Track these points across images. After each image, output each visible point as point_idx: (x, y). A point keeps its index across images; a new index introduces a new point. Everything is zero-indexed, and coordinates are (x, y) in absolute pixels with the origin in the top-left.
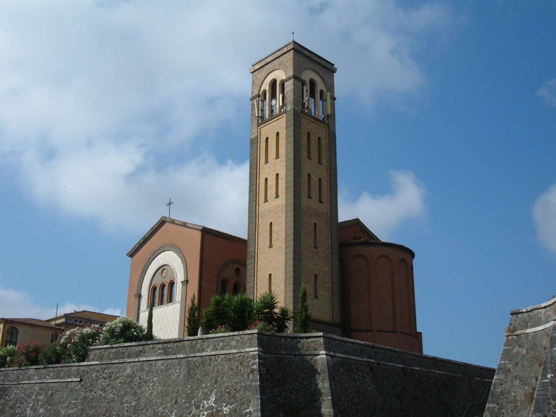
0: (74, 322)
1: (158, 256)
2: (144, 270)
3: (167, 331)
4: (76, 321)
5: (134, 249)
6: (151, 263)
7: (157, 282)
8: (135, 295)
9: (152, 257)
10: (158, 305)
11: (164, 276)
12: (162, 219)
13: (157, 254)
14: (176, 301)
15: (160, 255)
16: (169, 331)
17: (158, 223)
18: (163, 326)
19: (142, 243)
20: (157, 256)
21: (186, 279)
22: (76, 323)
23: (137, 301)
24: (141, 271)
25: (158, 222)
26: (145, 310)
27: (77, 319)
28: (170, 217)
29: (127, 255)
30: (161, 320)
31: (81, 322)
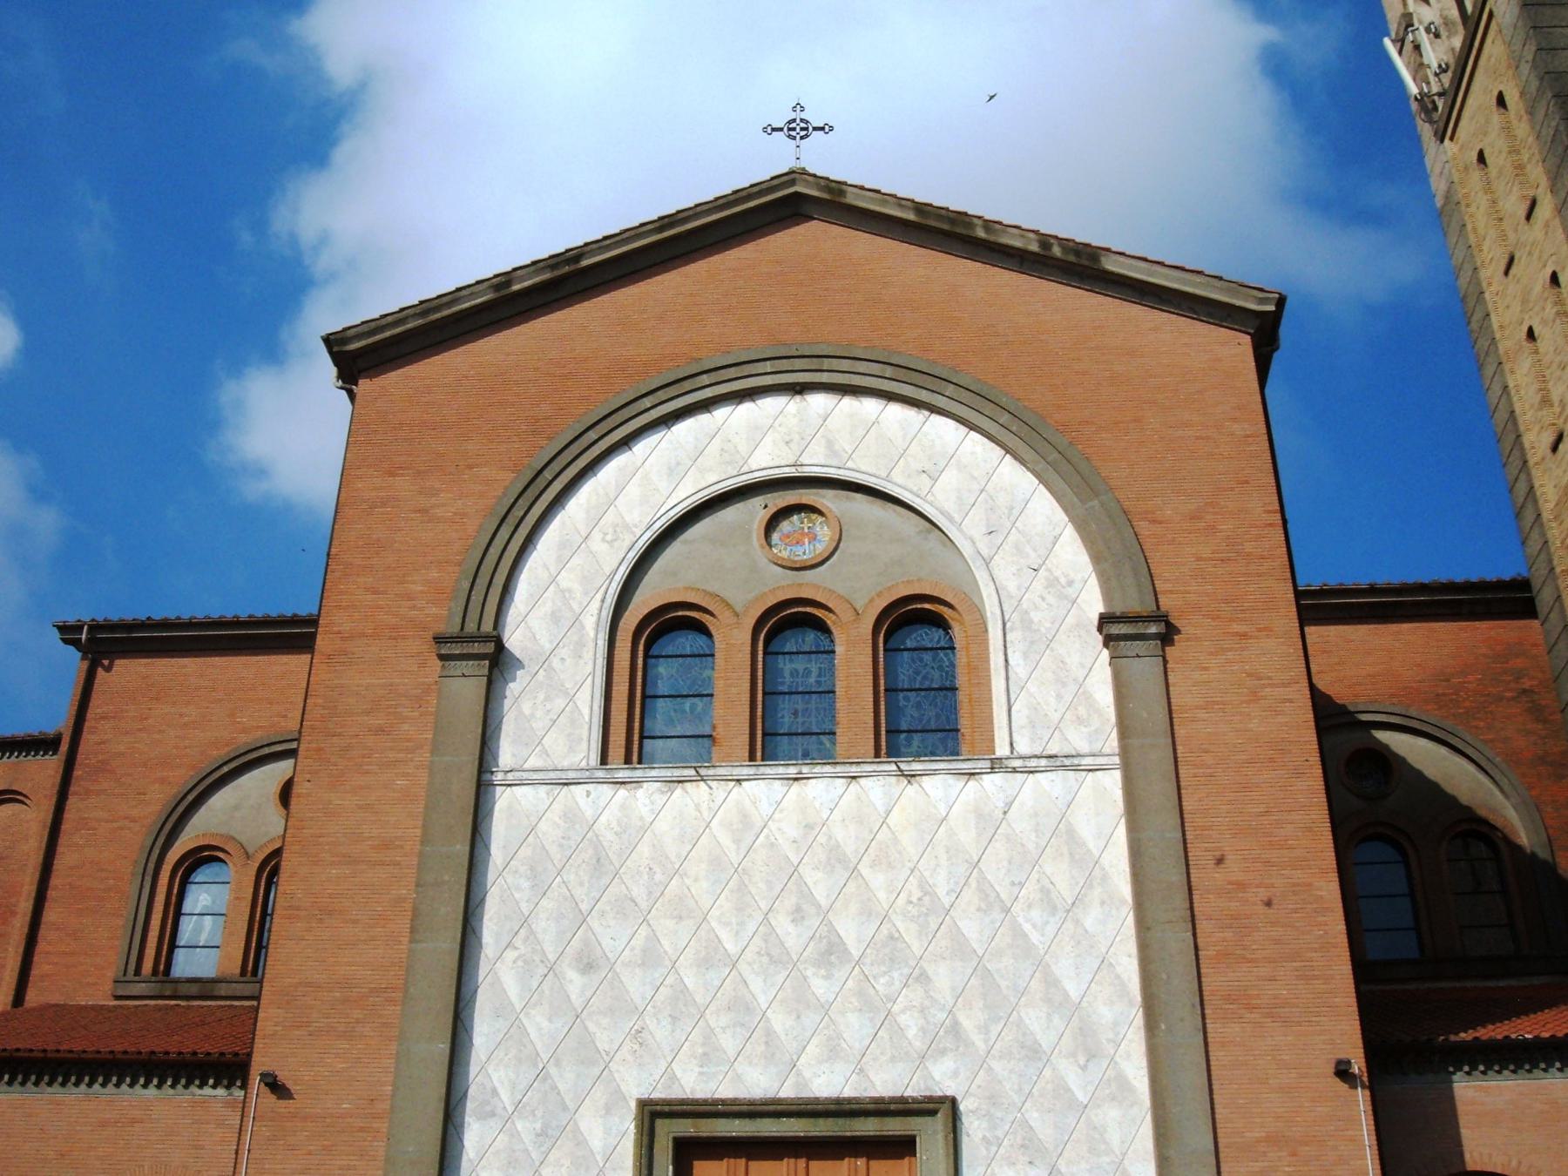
2: (548, 475)
6: (626, 443)
12: (793, 182)
16: (944, 977)
18: (851, 931)
26: (571, 775)
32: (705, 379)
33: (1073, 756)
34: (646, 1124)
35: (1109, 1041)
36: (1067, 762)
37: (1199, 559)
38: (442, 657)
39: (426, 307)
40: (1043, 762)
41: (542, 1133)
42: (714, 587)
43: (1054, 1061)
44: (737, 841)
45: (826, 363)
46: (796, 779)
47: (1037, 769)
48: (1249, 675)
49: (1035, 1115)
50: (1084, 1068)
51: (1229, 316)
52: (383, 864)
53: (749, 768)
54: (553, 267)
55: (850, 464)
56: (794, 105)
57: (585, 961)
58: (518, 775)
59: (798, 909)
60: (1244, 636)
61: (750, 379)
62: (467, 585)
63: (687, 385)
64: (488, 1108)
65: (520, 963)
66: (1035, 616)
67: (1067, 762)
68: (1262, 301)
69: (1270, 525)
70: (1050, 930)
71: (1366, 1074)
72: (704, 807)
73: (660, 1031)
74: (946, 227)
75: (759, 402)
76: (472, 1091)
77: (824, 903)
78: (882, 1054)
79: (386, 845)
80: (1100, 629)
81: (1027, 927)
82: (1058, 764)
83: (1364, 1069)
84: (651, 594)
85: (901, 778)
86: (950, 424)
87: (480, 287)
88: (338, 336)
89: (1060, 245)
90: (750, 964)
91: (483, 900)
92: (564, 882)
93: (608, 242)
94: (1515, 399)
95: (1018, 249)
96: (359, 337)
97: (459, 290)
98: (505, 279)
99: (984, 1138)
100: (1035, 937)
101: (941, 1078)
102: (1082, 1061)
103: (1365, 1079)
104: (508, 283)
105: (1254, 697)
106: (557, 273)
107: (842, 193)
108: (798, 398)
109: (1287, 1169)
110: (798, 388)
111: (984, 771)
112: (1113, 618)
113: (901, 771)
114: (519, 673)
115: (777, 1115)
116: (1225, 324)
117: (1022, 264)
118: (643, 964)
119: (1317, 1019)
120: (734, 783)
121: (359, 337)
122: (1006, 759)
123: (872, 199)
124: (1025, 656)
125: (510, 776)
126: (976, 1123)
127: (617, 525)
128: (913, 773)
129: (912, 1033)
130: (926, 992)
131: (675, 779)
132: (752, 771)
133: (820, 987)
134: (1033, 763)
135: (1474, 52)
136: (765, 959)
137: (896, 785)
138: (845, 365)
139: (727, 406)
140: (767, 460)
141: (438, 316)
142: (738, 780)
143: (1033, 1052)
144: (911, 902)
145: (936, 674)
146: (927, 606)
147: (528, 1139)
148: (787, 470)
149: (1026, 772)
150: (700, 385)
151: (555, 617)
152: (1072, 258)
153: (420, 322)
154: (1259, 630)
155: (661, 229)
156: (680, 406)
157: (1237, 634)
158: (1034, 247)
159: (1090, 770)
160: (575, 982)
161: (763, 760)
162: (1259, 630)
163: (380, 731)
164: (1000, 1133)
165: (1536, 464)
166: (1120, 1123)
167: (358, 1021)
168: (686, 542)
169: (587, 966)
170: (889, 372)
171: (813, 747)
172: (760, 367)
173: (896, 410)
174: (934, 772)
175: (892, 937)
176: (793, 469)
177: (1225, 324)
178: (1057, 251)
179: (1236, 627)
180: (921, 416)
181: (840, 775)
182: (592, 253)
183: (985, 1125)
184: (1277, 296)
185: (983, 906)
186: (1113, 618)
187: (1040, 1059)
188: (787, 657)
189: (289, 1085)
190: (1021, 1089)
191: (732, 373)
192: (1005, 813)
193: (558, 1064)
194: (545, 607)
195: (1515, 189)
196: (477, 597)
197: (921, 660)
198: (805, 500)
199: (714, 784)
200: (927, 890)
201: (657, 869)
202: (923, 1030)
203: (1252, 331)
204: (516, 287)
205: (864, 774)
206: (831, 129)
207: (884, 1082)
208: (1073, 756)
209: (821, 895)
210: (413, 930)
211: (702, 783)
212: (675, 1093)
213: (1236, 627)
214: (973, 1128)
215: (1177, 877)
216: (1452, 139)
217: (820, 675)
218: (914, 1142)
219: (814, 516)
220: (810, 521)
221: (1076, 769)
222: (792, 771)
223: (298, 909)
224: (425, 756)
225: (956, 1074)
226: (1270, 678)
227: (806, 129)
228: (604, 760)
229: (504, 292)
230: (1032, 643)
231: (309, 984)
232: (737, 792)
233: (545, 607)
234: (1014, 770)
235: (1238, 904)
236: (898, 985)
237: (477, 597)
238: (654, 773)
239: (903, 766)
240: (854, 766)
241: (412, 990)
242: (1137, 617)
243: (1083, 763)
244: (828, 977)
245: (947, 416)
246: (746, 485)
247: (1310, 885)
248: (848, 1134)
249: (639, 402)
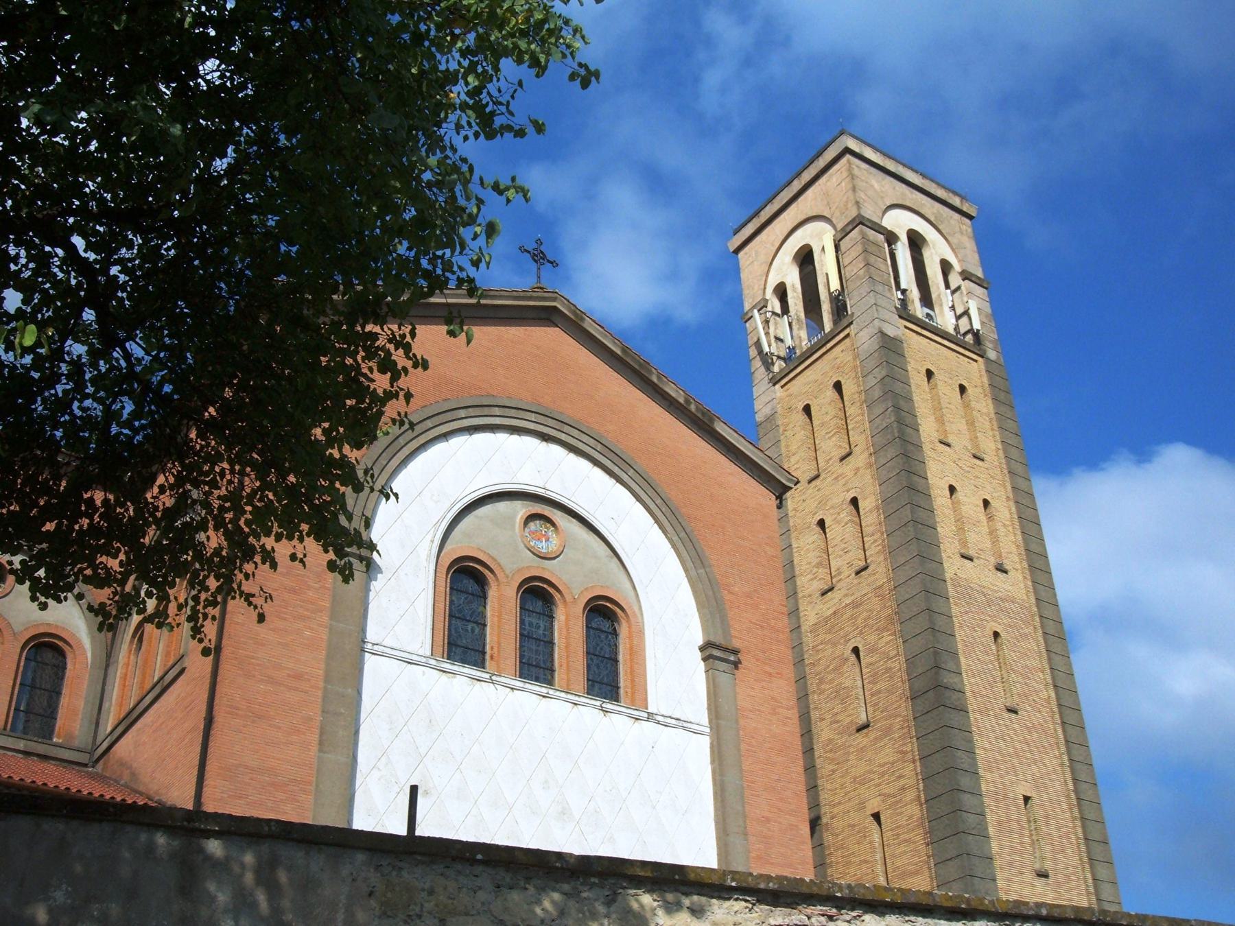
9: (462, 413)
26: (414, 657)
32: (497, 411)
36: (685, 725)
37: (751, 622)
40: (673, 721)
42: (494, 553)
45: (566, 429)
46: (544, 697)
51: (769, 481)
52: (296, 689)
58: (381, 649)
59: (546, 782)
60: (770, 674)
63: (486, 411)
67: (685, 725)
69: (783, 613)
75: (523, 437)
79: (298, 677)
80: (702, 649)
84: (459, 546)
89: (695, 405)
92: (409, 731)
94: (795, 555)
105: (774, 713)
107: (582, 319)
110: (546, 438)
114: (379, 576)
117: (669, 406)
123: (602, 333)
125: (376, 647)
132: (521, 684)
134: (668, 720)
135: (824, 350)
138: (575, 433)
142: (512, 689)
144: (606, 791)
145: (607, 649)
146: (608, 605)
152: (699, 415)
154: (778, 673)
157: (766, 672)
158: (681, 400)
161: (520, 677)
162: (778, 673)
163: (292, 591)
165: (804, 597)
167: (282, 801)
168: (476, 516)
170: (599, 447)
171: (542, 676)
174: (619, 713)
176: (543, 491)
178: (693, 408)
179: (767, 668)
188: (527, 612)
191: (512, 413)
195: (834, 439)
197: (599, 637)
198: (546, 513)
210: (321, 743)
213: (767, 668)
216: (782, 387)
217: (545, 630)
219: (548, 525)
220: (546, 528)
222: (544, 690)
223: (237, 708)
224: (325, 619)
226: (781, 703)
227: (543, 259)
231: (247, 767)
234: (658, 723)
241: (321, 786)
247: (796, 826)
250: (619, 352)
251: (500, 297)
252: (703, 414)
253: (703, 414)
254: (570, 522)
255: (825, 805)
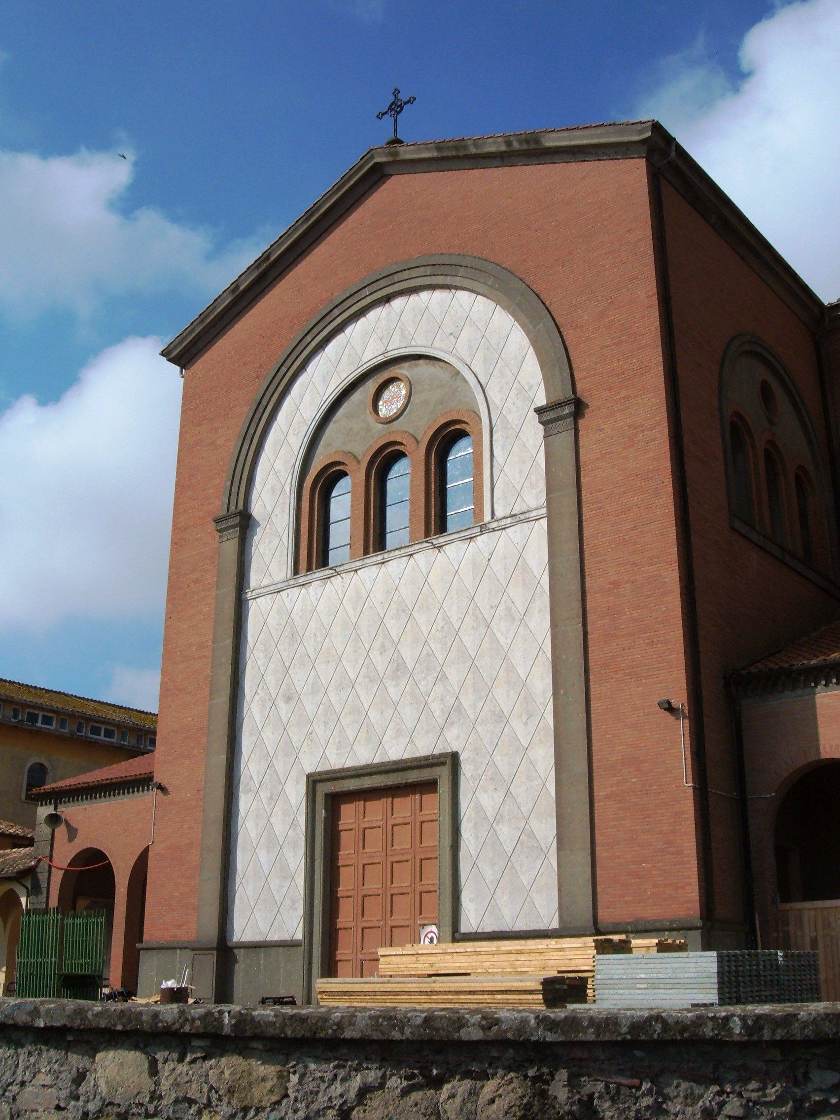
0: (91, 734)
1: (349, 330)
2: (264, 402)
3: (442, 677)
4: (96, 731)
5: (202, 321)
6: (303, 367)
7: (348, 448)
8: (217, 521)
9: (309, 338)
10: (366, 552)
11: (386, 409)
12: (372, 157)
13: (339, 320)
14: (499, 514)
15: (362, 321)
16: (454, 675)
17: (344, 184)
18: (408, 654)
19: (245, 291)
20: (340, 328)
21: (563, 392)
22: (98, 737)
23: (231, 546)
24: (246, 411)
25: (345, 179)
26: (280, 586)
27: (98, 725)
28: (348, 545)
29: (162, 354)
30: (393, 626)
31: (109, 734)
33: (525, 513)
34: (311, 787)
35: (541, 704)
36: (522, 517)
38: (219, 531)
39: (203, 316)
40: (509, 520)
41: (270, 799)
43: (510, 722)
44: (354, 609)
46: (383, 563)
47: (506, 526)
48: (629, 427)
49: (499, 758)
50: (526, 724)
53: (358, 562)
54: (258, 267)
55: (413, 343)
56: (393, 91)
57: (287, 696)
59: (383, 646)
61: (359, 303)
62: (229, 483)
63: (328, 319)
64: (248, 787)
65: (260, 702)
66: (510, 418)
67: (522, 517)
68: (641, 131)
70: (511, 635)
71: (687, 708)
72: (339, 592)
73: (320, 731)
74: (454, 153)
76: (242, 779)
77: (396, 639)
78: (422, 730)
81: (498, 635)
82: (517, 520)
83: (686, 704)
85: (435, 549)
86: (466, 293)
87: (225, 294)
88: (166, 351)
90: (360, 684)
91: (245, 669)
93: (282, 239)
95: (495, 153)
96: (176, 347)
97: (215, 300)
98: (235, 285)
99: (472, 775)
100: (502, 641)
101: (452, 741)
102: (524, 719)
103: (686, 711)
104: (237, 287)
106: (261, 270)
108: (387, 305)
109: (633, 780)
111: (477, 534)
112: (543, 409)
113: (435, 545)
115: (370, 774)
116: (627, 156)
118: (312, 693)
119: (658, 672)
120: (353, 572)
121: (176, 347)
122: (489, 523)
124: (503, 447)
126: (468, 767)
127: (300, 423)
128: (440, 545)
129: (437, 713)
130: (445, 686)
131: (325, 577)
133: (394, 692)
136: (367, 680)
137: (432, 553)
139: (351, 325)
140: (371, 355)
141: (208, 321)
143: (501, 719)
144: (438, 630)
147: (265, 801)
148: (380, 358)
149: (501, 529)
150: (334, 317)
151: (273, 490)
153: (201, 327)
155: (307, 220)
156: (330, 330)
158: (503, 148)
159: (537, 519)
160: (284, 709)
164: (480, 772)
166: (544, 758)
169: (288, 699)
170: (429, 270)
172: (414, 273)
173: (438, 294)
174: (451, 542)
175: (428, 655)
176: (382, 357)
177: (627, 156)
178: (516, 145)
180: (451, 294)
181: (404, 555)
182: (275, 251)
183: (472, 767)
184: (651, 123)
185: (475, 625)
186: (543, 409)
187: (502, 721)
189: (168, 787)
190: (491, 742)
192: (489, 560)
193: (276, 758)
194: (268, 487)
196: (235, 489)
199: (344, 575)
200: (447, 621)
201: (318, 635)
202: (442, 711)
203: (644, 155)
204: (242, 288)
205: (415, 552)
206: (415, 99)
207: (424, 747)
208: (525, 513)
209: (394, 634)
211: (339, 576)
212: (327, 767)
214: (467, 770)
215: (576, 587)
218: (436, 783)
221: (527, 520)
225: (458, 737)
226: (642, 426)
228: (296, 571)
229: (238, 292)
230: (507, 437)
232: (355, 578)
233: (268, 487)
234: (494, 530)
235: (613, 598)
236: (431, 685)
237: (235, 489)
238: (316, 576)
239: (435, 542)
240: (410, 547)
242: (556, 405)
243: (531, 516)
244: (397, 685)
245: (464, 290)
246: (362, 375)
248: (404, 781)
249: (304, 340)
250: (435, 154)
251: (324, 203)
252: (527, 141)
253: (527, 141)
254: (416, 366)
255: (154, 1071)
